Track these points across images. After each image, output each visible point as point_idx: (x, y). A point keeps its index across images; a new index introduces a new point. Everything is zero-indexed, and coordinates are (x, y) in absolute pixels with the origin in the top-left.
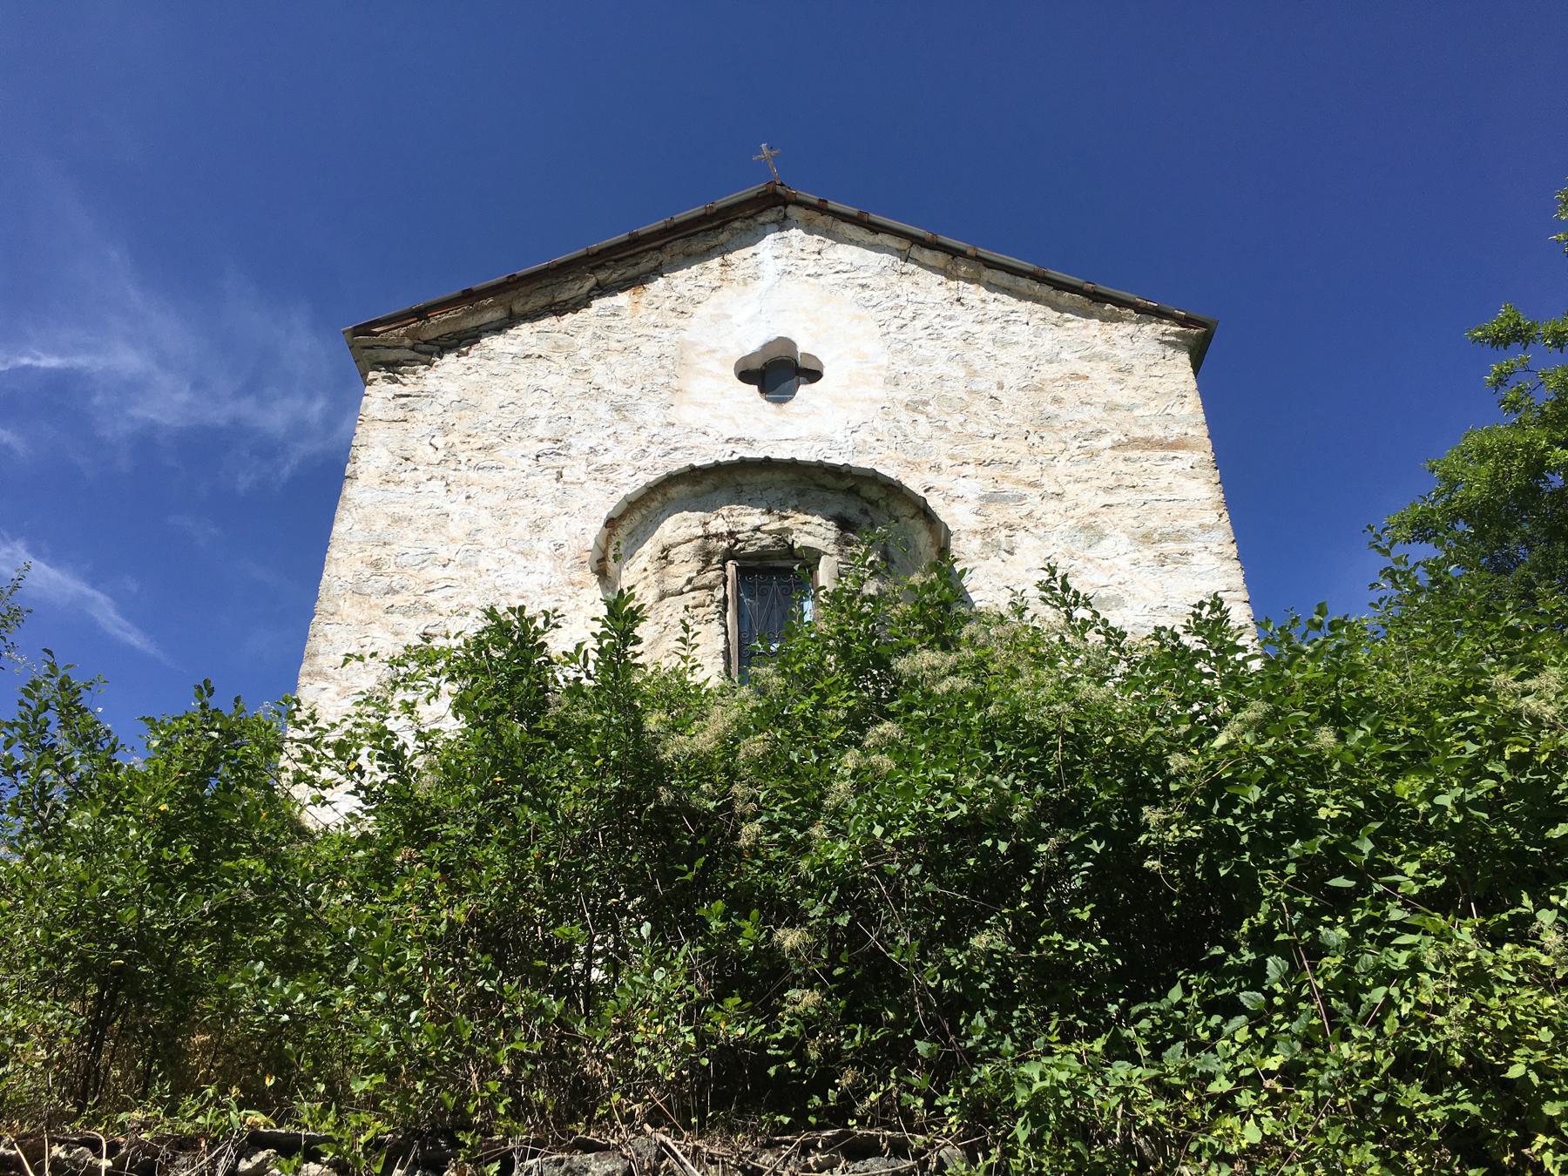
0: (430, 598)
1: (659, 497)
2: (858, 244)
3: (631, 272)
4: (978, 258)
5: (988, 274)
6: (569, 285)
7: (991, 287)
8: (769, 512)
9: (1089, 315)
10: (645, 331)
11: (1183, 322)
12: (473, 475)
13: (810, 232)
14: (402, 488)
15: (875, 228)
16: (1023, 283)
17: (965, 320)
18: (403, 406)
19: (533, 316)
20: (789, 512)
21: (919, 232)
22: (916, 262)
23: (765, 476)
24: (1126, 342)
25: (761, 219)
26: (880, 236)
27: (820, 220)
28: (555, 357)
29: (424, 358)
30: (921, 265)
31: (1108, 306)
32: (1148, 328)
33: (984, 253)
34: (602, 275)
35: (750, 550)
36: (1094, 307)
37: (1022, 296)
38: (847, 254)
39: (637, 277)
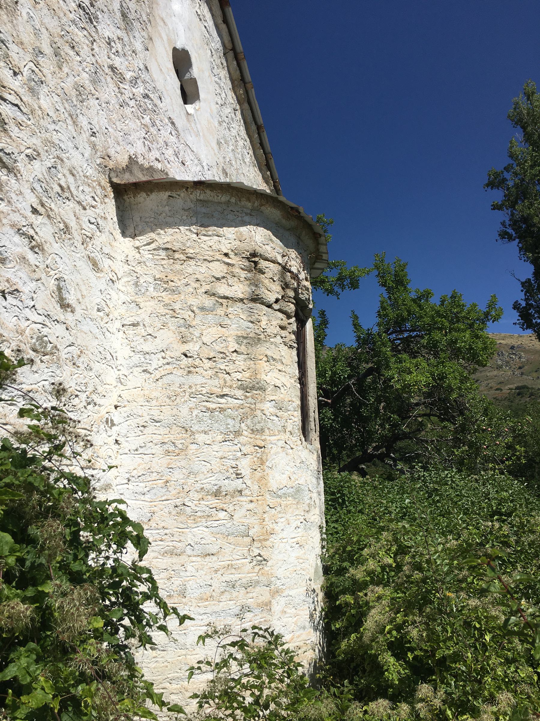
1: (256, 204)
5: (246, 106)
9: (260, 170)
16: (254, 127)
31: (268, 173)
33: (253, 93)
36: (264, 168)
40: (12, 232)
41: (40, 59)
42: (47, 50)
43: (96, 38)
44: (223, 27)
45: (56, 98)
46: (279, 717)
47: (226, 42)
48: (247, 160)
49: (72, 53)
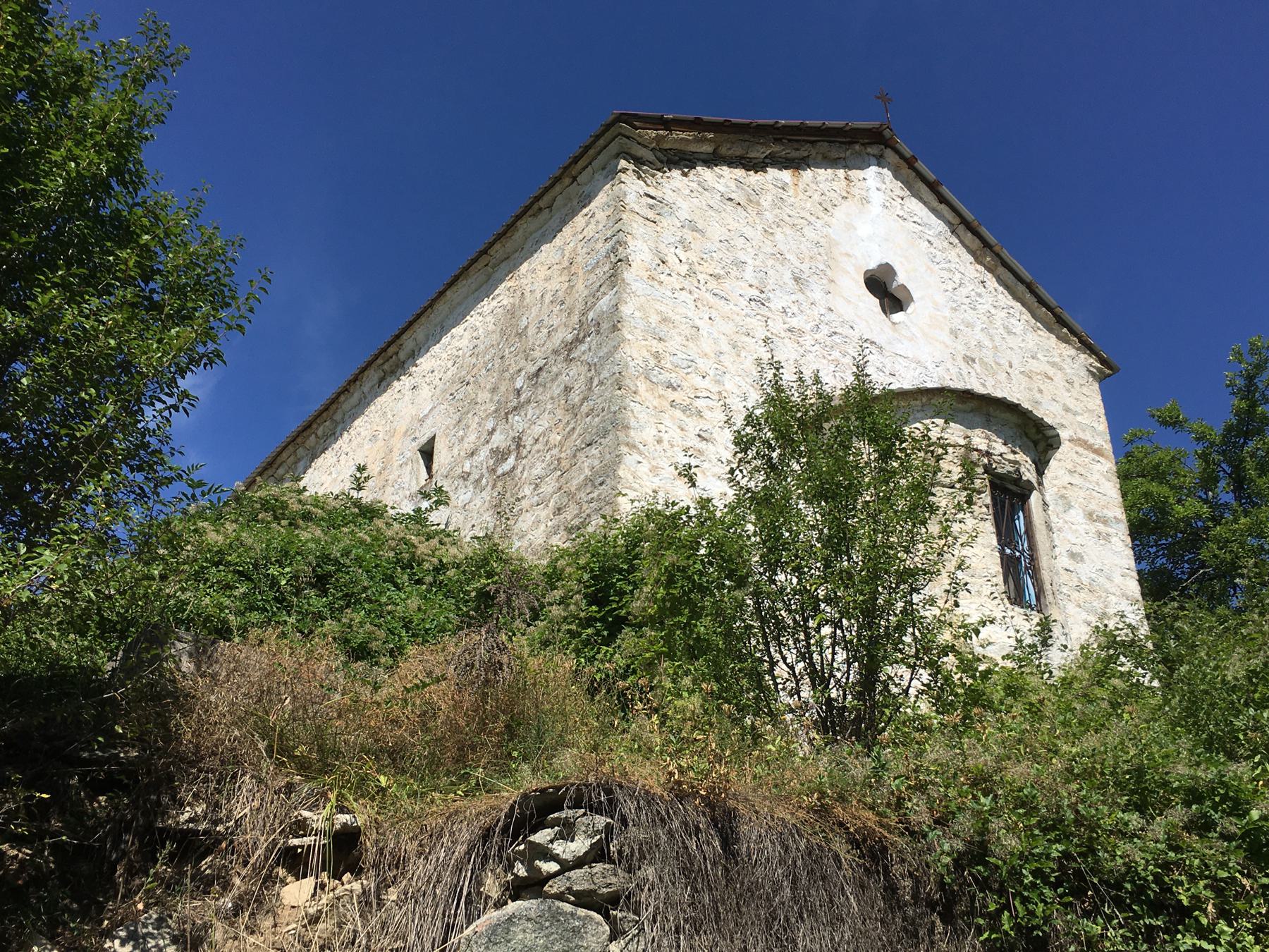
0: (700, 403)
1: (924, 400)
2: (925, 203)
3: (794, 154)
4: (998, 255)
5: (1001, 270)
6: (759, 147)
7: (1000, 281)
8: (1005, 444)
9: (1050, 330)
10: (808, 216)
11: (1103, 361)
12: (709, 296)
13: (896, 177)
14: (662, 290)
15: (942, 199)
16: (1021, 288)
17: (986, 303)
18: (651, 207)
19: (732, 162)
20: (1017, 450)
21: (969, 216)
22: (958, 237)
23: (1008, 416)
24: (1069, 360)
25: (869, 150)
26: (943, 206)
27: (906, 171)
28: (750, 209)
29: (659, 165)
30: (961, 242)
31: (1065, 330)
32: (1083, 356)
33: (1005, 254)
34: (776, 148)
35: (1000, 471)
36: (1056, 326)
37: (1016, 297)
38: (915, 205)
39: (792, 160)
40: (714, 479)
41: (722, 358)
42: (725, 347)
43: (769, 314)
44: (943, 208)
45: (738, 378)
46: (502, 495)
47: (951, 219)
48: (1019, 327)
49: (747, 339)
